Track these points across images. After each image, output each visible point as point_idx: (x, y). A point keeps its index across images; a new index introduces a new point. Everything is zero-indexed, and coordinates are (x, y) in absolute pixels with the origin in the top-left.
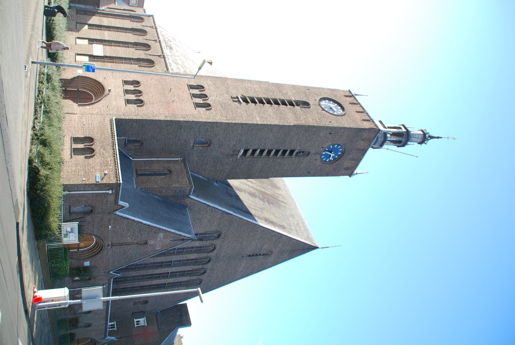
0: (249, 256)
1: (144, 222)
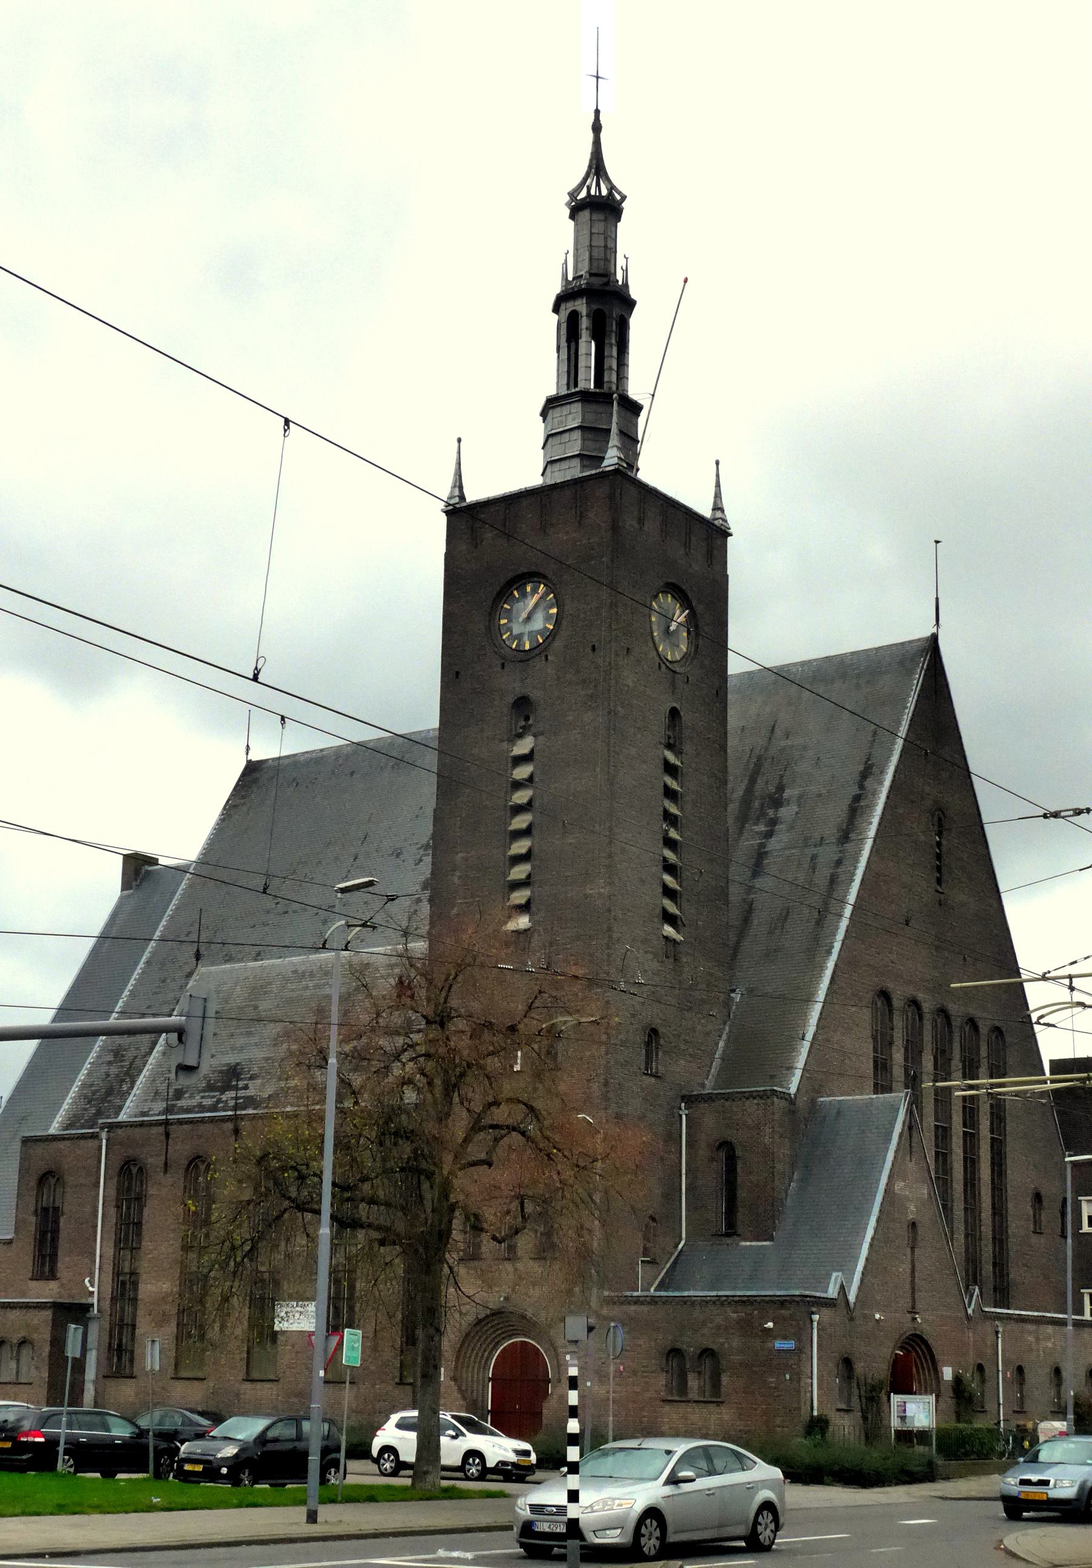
0: (939, 881)
1: (870, 1233)
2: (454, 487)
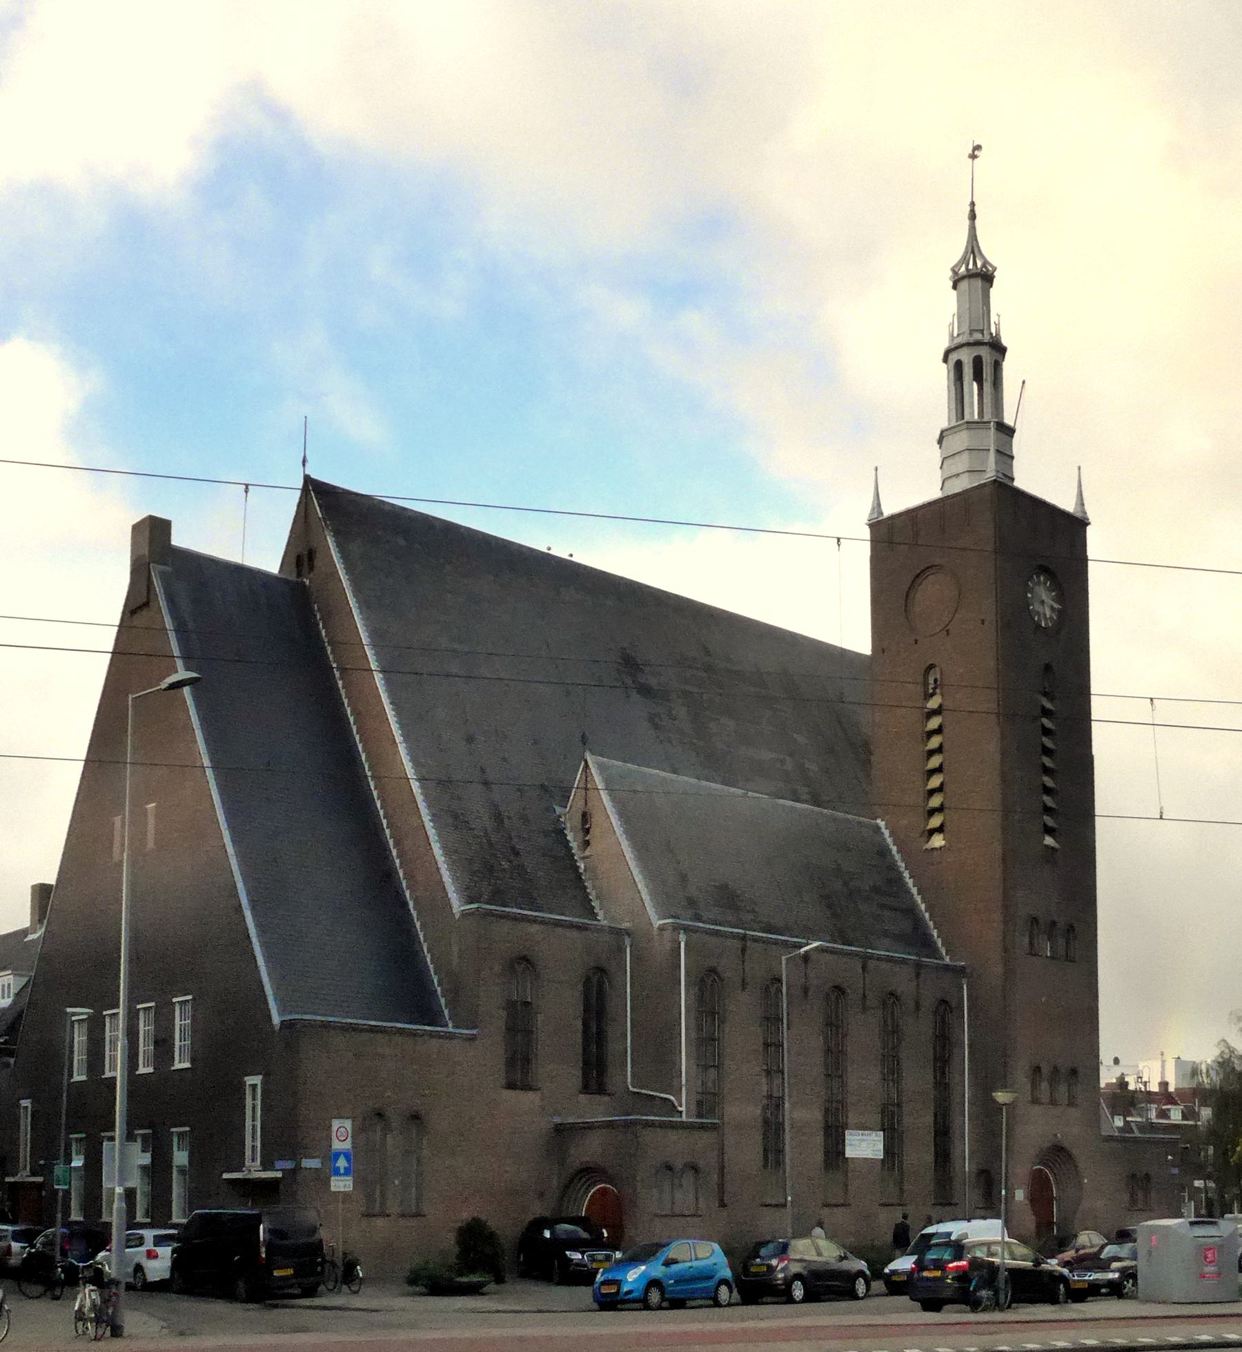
2: (873, 509)
